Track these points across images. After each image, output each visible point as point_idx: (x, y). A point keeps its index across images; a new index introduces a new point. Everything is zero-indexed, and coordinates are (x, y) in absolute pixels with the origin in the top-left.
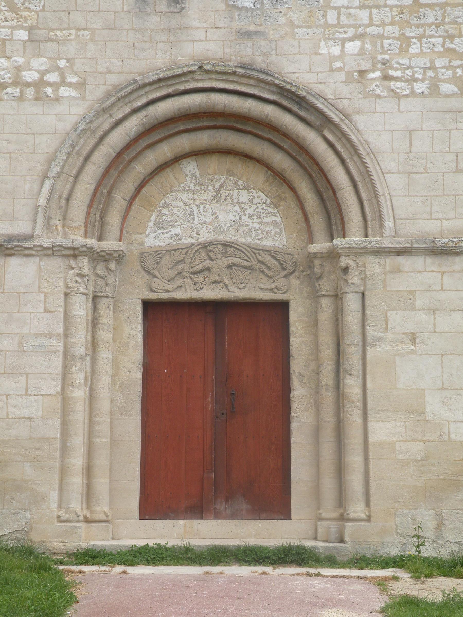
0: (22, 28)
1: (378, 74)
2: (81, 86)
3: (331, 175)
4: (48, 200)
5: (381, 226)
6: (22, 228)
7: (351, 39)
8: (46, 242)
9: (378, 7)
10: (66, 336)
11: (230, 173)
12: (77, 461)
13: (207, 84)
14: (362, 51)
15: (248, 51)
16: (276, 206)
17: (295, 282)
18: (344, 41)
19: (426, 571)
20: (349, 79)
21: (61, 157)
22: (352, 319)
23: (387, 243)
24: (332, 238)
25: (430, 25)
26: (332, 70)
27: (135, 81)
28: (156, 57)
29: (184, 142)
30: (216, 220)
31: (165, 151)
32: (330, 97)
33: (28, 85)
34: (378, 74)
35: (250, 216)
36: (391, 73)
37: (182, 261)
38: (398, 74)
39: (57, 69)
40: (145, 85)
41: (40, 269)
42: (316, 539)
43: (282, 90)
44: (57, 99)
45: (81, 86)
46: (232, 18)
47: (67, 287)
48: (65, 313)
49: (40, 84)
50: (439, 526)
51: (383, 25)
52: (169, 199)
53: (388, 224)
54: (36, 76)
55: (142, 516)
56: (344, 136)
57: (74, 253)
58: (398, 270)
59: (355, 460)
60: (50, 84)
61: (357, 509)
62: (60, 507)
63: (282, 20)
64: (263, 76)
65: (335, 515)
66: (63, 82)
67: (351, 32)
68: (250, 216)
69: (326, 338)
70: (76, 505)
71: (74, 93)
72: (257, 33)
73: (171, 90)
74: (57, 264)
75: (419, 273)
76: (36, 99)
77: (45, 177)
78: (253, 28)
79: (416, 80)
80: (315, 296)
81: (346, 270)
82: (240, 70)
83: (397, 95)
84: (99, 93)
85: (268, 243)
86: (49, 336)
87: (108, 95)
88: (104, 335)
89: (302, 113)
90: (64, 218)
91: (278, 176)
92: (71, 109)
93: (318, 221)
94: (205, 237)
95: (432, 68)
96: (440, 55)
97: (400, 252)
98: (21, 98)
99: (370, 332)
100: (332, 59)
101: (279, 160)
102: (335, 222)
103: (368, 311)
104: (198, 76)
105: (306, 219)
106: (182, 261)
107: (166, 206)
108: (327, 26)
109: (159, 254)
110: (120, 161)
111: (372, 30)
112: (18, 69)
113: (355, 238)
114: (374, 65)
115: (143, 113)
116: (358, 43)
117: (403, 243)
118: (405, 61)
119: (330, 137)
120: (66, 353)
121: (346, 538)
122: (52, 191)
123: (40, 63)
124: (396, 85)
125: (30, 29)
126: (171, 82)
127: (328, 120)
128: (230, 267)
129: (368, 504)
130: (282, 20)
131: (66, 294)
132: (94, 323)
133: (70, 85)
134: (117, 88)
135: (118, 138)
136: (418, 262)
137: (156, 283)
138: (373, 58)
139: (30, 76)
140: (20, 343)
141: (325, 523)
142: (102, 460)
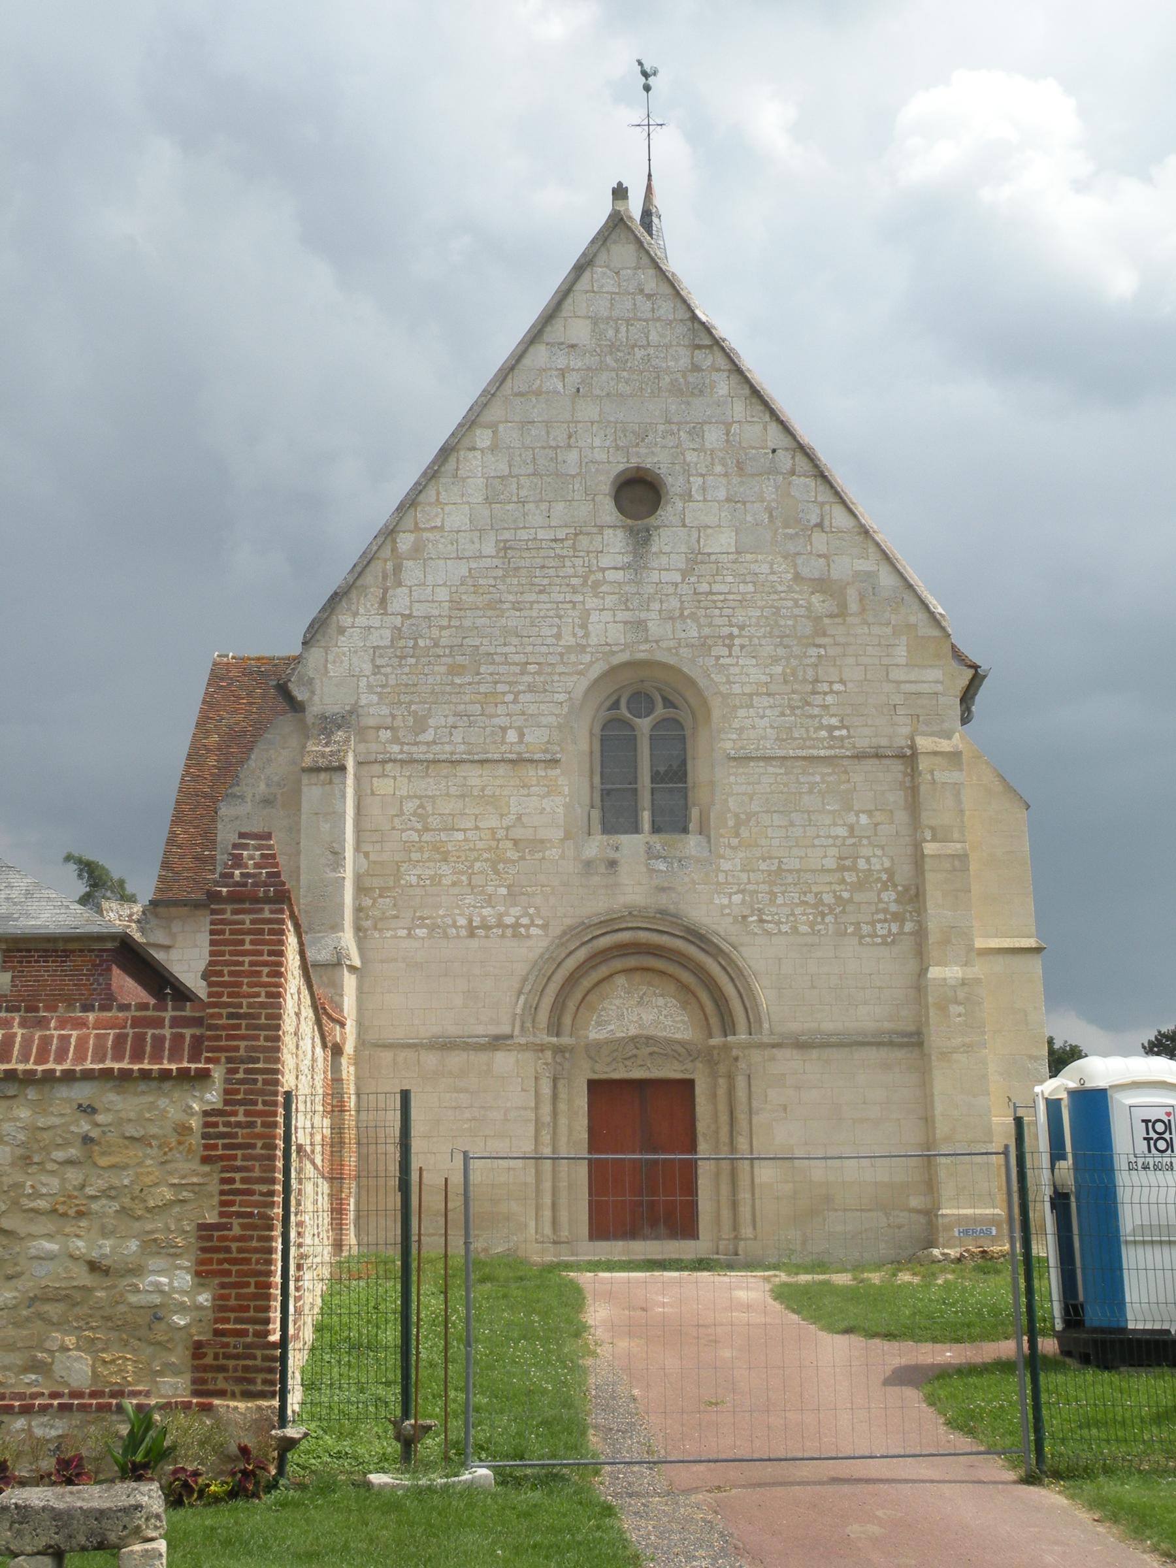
0: (502, 886)
1: (755, 918)
2: (545, 927)
3: (724, 989)
4: (523, 1010)
5: (761, 1026)
6: (505, 1029)
7: (736, 893)
8: (523, 1041)
9: (753, 871)
10: (537, 1108)
11: (650, 984)
12: (547, 1200)
13: (635, 925)
14: (744, 902)
15: (664, 901)
16: (684, 1009)
17: (699, 1065)
18: (730, 895)
19: (795, 1270)
20: (735, 921)
21: (532, 978)
22: (741, 1094)
23: (766, 1040)
24: (726, 1036)
25: (790, 884)
26: (723, 915)
27: (583, 923)
28: (598, 905)
29: (618, 964)
30: (640, 1019)
31: (604, 971)
32: (722, 934)
33: (508, 926)
34: (755, 918)
35: (666, 1016)
36: (764, 917)
37: (616, 1050)
38: (769, 918)
39: (527, 914)
40: (590, 926)
41: (517, 1061)
42: (717, 1253)
43: (688, 930)
44: (528, 936)
45: (545, 927)
46: (651, 877)
47: (537, 1072)
48: (536, 1092)
49: (516, 926)
50: (804, 1243)
51: (757, 883)
52: (606, 1004)
53: (766, 1026)
54: (513, 920)
55: (591, 1238)
56: (732, 961)
57: (541, 1048)
58: (773, 1059)
59: (744, 1195)
60: (524, 926)
61: (747, 1231)
62: (536, 1232)
63: (687, 879)
64: (674, 920)
65: (732, 1236)
66: (532, 924)
67: (735, 888)
68: (666, 1016)
69: (722, 1106)
70: (548, 1231)
71: (540, 932)
72: (669, 888)
73: (609, 929)
74: (529, 1056)
75: (788, 1062)
76: (514, 936)
77: (520, 993)
78: (666, 885)
79: (782, 923)
80: (714, 1075)
81: (736, 1059)
82: (658, 916)
83: (768, 933)
84: (558, 932)
85: (678, 1036)
86: (525, 1109)
87: (564, 933)
88: (562, 1106)
89: (703, 946)
90: (533, 1021)
91: (685, 987)
92: (538, 942)
93: (714, 1021)
94: (633, 1031)
95: (793, 914)
96: (798, 905)
97: (774, 1046)
98: (503, 936)
99: (755, 1104)
100: (723, 907)
101: (686, 977)
102: (728, 1025)
103: (753, 1089)
104: (628, 919)
105: (706, 1019)
106: (616, 1050)
107: (604, 1009)
108: (718, 883)
109: (599, 1045)
110: (572, 980)
111: (750, 887)
112: (501, 916)
113: (743, 1037)
114: (753, 911)
115: (590, 945)
116: (740, 896)
117: (775, 1039)
118: (774, 909)
119: (723, 962)
120: (537, 1120)
121: (740, 1252)
122: (525, 1003)
123: (516, 911)
124: (769, 927)
125: (509, 887)
126: (609, 924)
127: (721, 951)
128: (651, 1054)
129: (754, 1228)
130: (687, 879)
131: (536, 1078)
132: (555, 1097)
133: (537, 926)
134: (571, 928)
135: (571, 964)
136: (787, 1053)
137: (598, 1067)
138: (752, 907)
139: (509, 920)
140: (505, 1115)
141: (724, 1242)
142: (563, 1200)
